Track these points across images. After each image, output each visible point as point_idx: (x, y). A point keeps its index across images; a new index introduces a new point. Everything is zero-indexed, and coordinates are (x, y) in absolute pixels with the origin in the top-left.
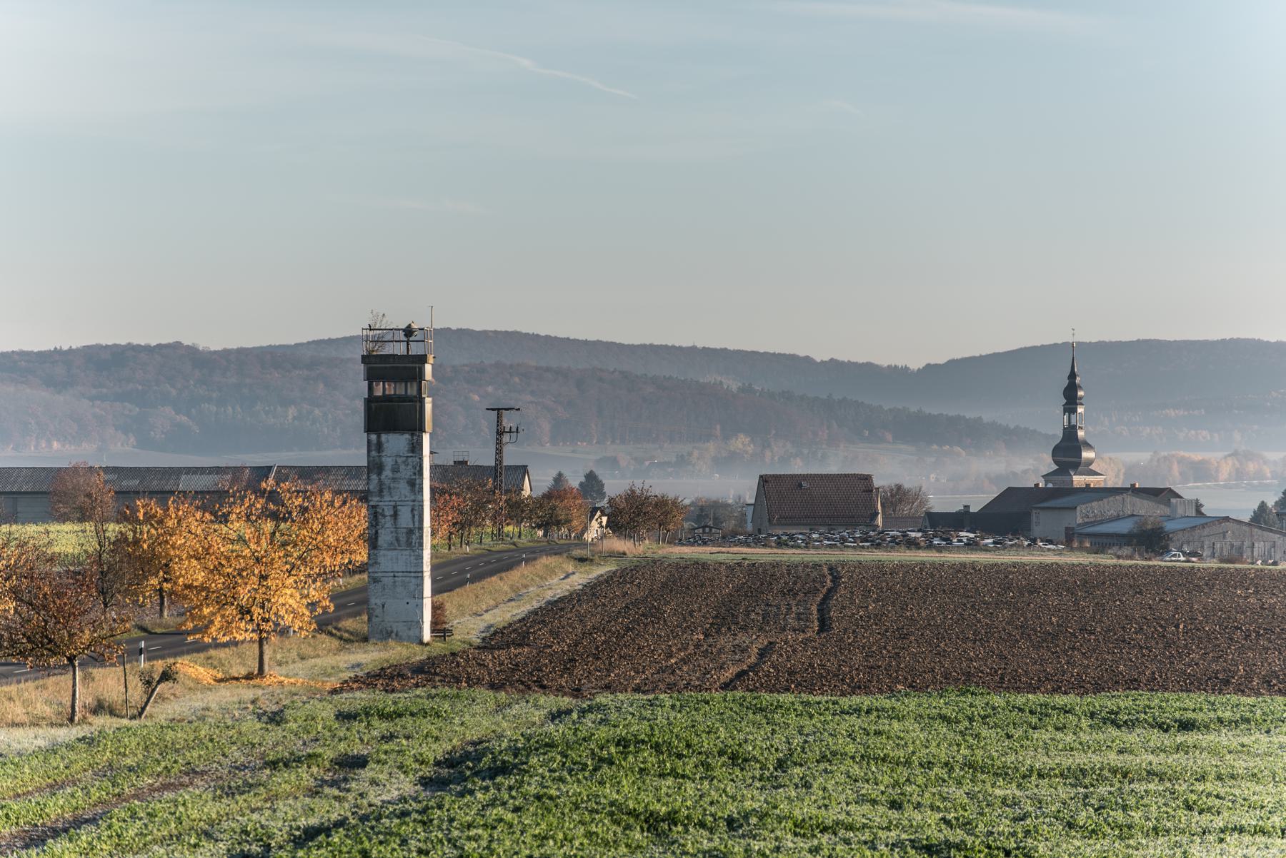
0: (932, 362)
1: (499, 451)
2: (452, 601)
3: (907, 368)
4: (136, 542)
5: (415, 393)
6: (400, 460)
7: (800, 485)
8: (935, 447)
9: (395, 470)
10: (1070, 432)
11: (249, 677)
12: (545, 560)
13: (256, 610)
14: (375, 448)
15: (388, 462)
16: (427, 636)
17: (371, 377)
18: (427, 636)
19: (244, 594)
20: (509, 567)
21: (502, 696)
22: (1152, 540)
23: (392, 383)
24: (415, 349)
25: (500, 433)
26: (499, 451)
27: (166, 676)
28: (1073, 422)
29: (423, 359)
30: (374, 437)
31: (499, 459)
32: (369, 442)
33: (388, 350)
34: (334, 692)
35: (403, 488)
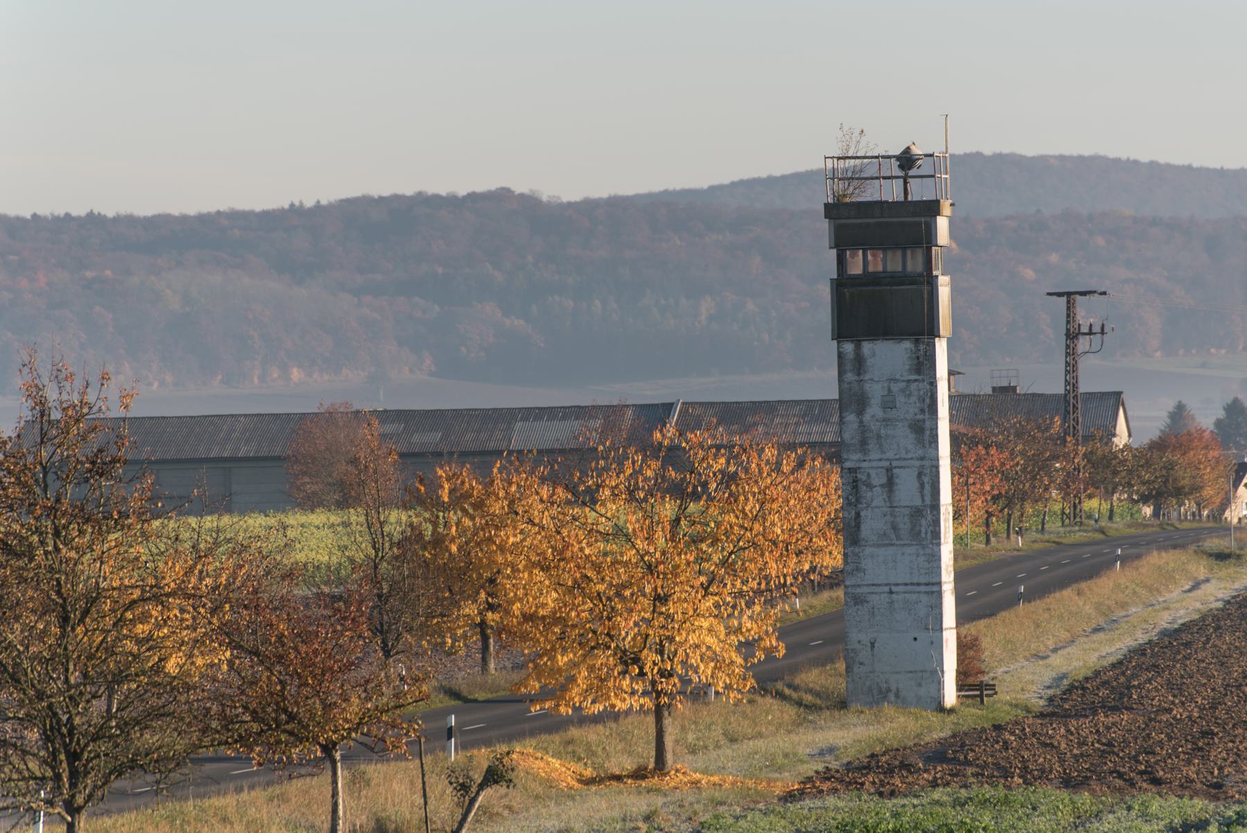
1: (1071, 368)
2: (992, 634)
4: (438, 542)
6: (895, 388)
11: (639, 774)
12: (1156, 559)
13: (649, 657)
15: (875, 392)
16: (950, 696)
17: (843, 241)
18: (950, 696)
19: (627, 630)
20: (1093, 571)
21: (1085, 799)
22: (843, 725)
23: (876, 249)
24: (920, 191)
25: (1072, 336)
26: (1071, 368)
27: (494, 776)
29: (933, 208)
30: (849, 347)
31: (1072, 384)
33: (871, 193)
34: (789, 797)
35: (904, 438)
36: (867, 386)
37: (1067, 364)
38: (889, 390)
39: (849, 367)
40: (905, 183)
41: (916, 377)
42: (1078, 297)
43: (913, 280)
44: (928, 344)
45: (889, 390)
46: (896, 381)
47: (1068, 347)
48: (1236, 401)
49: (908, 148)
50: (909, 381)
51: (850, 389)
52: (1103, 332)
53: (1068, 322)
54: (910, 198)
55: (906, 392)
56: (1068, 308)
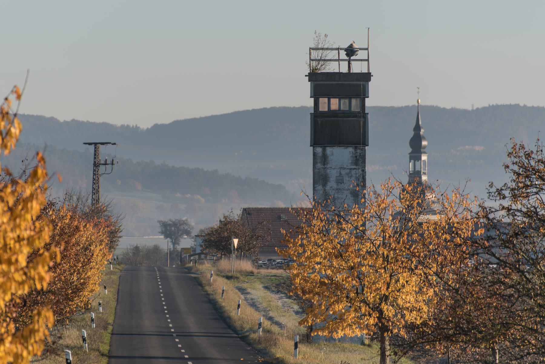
0: (160, 122)
3: (137, 128)
5: (358, 110)
6: (344, 172)
7: (280, 218)
8: (178, 195)
9: (340, 181)
10: (415, 175)
14: (320, 162)
15: (333, 174)
24: (358, 68)
28: (417, 168)
30: (319, 150)
32: (315, 154)
33: (332, 68)
36: (328, 171)
37: (94, 179)
38: (340, 173)
39: (319, 160)
40: (349, 64)
41: (355, 167)
42: (100, 146)
43: (355, 115)
44: (362, 150)
45: (340, 173)
46: (344, 168)
47: (94, 170)
48: (245, 210)
49: (352, 45)
50: (351, 169)
51: (319, 172)
52: (112, 164)
53: (95, 158)
54: (351, 72)
55: (349, 175)
56: (95, 151)
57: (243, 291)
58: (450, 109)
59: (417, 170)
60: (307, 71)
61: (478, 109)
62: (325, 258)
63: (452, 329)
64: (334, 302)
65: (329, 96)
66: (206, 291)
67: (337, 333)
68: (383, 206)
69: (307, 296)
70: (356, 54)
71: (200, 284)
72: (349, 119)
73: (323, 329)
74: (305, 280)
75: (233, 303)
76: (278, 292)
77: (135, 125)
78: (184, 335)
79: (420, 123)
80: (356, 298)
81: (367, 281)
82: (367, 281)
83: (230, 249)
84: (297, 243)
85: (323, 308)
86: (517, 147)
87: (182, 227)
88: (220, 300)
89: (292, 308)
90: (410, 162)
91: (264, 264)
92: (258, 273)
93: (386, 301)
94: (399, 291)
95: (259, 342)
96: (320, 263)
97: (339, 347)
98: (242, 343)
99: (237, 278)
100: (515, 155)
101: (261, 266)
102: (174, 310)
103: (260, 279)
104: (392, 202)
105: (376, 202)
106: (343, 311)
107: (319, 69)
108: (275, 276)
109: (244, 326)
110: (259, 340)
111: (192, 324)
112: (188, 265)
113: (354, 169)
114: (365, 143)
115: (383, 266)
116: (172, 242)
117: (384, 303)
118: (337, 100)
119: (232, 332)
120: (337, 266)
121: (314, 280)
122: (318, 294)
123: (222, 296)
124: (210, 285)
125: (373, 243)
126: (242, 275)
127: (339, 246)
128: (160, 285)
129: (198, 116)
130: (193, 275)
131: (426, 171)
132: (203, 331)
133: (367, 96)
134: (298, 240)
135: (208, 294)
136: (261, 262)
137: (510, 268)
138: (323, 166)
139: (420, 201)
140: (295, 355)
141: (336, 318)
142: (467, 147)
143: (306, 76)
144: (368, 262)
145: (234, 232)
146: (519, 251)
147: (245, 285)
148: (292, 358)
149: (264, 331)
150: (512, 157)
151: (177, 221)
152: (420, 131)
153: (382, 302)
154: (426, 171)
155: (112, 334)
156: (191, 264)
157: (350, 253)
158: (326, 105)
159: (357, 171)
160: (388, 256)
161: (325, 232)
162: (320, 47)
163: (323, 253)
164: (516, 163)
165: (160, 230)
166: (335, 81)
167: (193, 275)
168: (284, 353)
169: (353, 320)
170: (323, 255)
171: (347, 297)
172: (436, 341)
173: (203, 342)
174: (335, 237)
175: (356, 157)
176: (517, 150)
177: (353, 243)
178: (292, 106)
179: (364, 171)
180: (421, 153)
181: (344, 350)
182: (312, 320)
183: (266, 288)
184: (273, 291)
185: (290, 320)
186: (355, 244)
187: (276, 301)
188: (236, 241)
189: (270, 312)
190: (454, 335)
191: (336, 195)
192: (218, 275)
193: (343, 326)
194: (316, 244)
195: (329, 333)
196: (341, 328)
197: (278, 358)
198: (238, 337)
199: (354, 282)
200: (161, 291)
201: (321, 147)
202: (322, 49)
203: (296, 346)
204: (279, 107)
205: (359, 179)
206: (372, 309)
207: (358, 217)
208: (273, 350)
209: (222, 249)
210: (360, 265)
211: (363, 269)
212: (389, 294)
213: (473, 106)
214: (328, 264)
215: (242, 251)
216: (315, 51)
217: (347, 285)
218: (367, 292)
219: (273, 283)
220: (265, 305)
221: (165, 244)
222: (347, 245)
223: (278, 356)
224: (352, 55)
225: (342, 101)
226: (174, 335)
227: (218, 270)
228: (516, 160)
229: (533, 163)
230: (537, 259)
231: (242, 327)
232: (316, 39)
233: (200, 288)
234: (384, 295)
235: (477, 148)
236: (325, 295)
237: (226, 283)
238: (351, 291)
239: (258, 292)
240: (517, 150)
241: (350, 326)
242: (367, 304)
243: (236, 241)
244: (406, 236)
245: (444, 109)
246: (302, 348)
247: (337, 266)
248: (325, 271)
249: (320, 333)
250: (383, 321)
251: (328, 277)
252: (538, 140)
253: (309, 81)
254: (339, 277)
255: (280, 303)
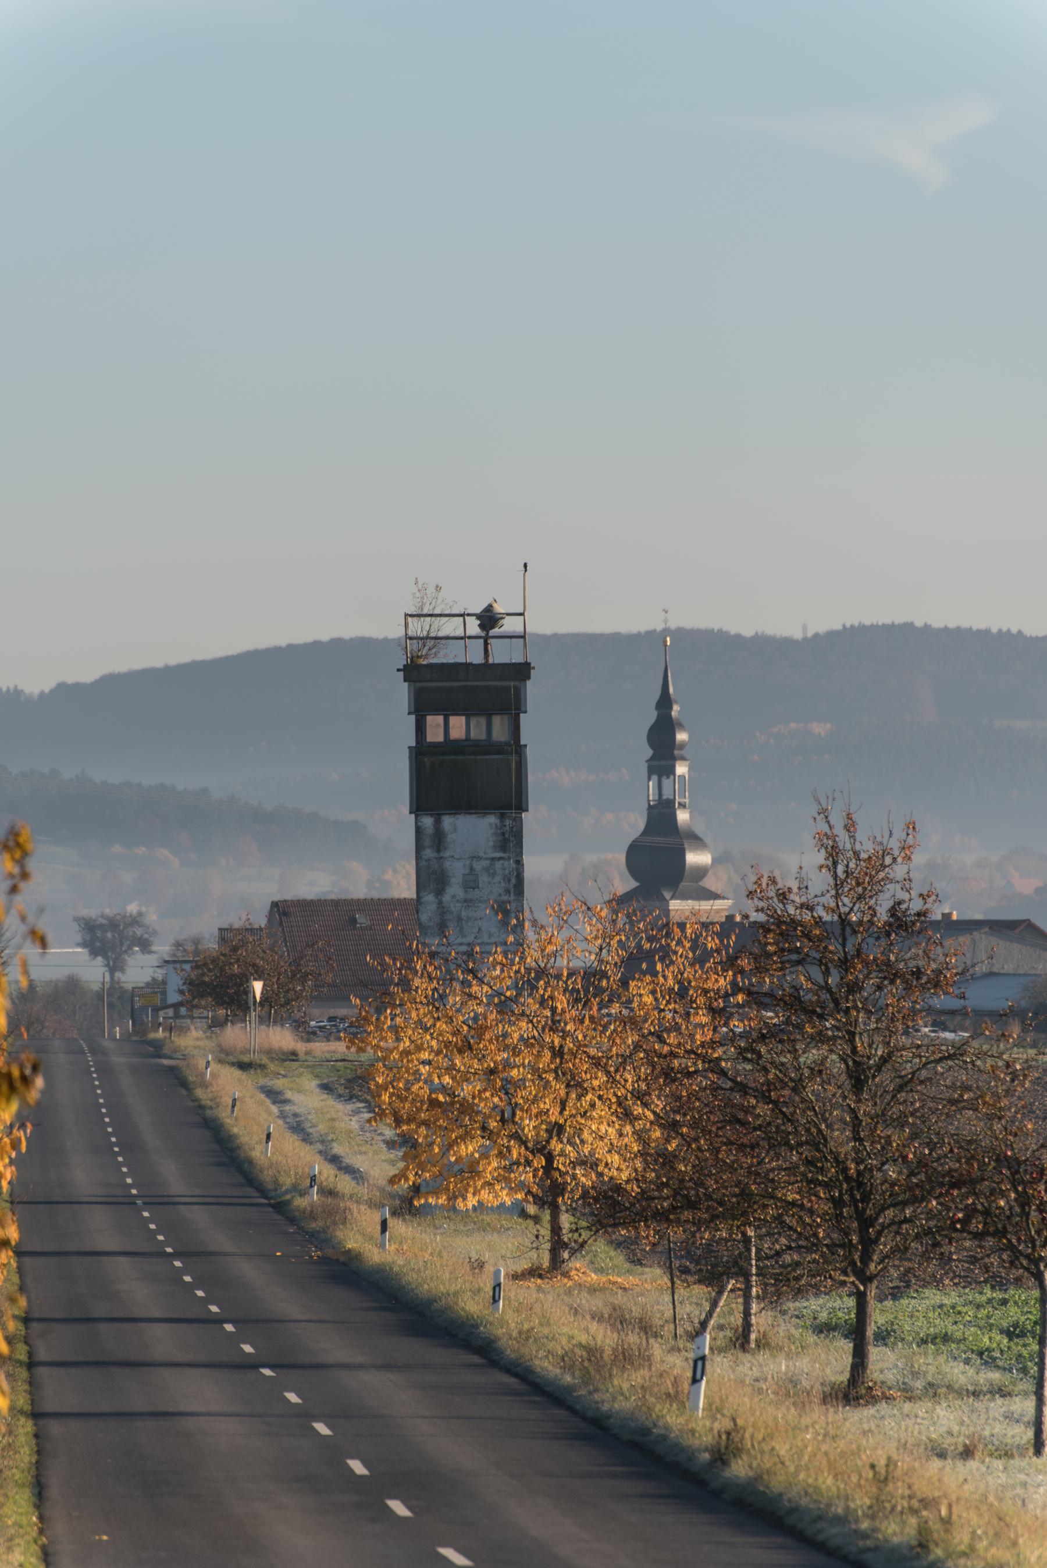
0: (70, 679)
3: (17, 693)
6: (478, 866)
7: (353, 921)
9: (470, 883)
10: (661, 815)
14: (430, 846)
15: (456, 869)
23: (467, 721)
24: (502, 654)
28: (667, 794)
30: (428, 821)
32: (418, 830)
36: (447, 864)
39: (427, 842)
40: (486, 644)
43: (498, 749)
44: (515, 820)
46: (479, 858)
48: (275, 905)
49: (490, 606)
50: (493, 859)
54: (491, 661)
57: (274, 1096)
58: (752, 638)
59: (665, 797)
60: (401, 663)
61: (816, 636)
62: (438, 1053)
63: (668, 1198)
64: (456, 1138)
65: (447, 710)
66: (197, 1100)
67: (465, 1199)
68: (550, 949)
69: (405, 1128)
70: (500, 623)
71: (184, 1084)
72: (488, 757)
73: (436, 1193)
74: (399, 1097)
75: (255, 1128)
76: (351, 1098)
77: (12, 687)
78: (160, 1202)
79: (671, 691)
80: (500, 1131)
81: (522, 1097)
82: (522, 1097)
83: (247, 1003)
84: (384, 1023)
85: (437, 1150)
86: (764, 881)
87: (130, 931)
88: (228, 1121)
89: (381, 1134)
90: (649, 779)
91: (320, 1027)
92: (307, 1053)
93: (559, 1135)
94: (584, 1115)
95: (313, 1216)
96: (429, 1063)
97: (475, 1223)
98: (277, 1217)
99: (262, 1067)
100: (759, 896)
101: (314, 1033)
102: (132, 1146)
103: (315, 1067)
104: (568, 942)
105: (537, 941)
106: (477, 1155)
107: (426, 656)
108: (344, 1060)
109: (281, 1179)
110: (312, 1212)
111: (173, 1178)
112: (152, 1036)
113: (501, 858)
114: (521, 806)
115: (553, 1066)
116: (107, 965)
117: (555, 1139)
118: (463, 718)
119: (256, 1194)
120: (462, 1068)
121: (417, 1095)
122: (425, 1123)
123: (233, 1111)
124: (205, 1085)
125: (531, 1021)
126: (272, 1059)
127: (465, 1028)
128: (98, 1087)
129: (159, 664)
130: (166, 1062)
131: (687, 801)
132: (198, 1192)
133: (523, 709)
134: (386, 1018)
135: (201, 1107)
136: (313, 1023)
137: (755, 1097)
138: (436, 855)
139: (623, 938)
140: (382, 1246)
141: (462, 1171)
142: (793, 725)
143: (398, 670)
144: (524, 1059)
145: (254, 965)
146: (769, 1066)
147: (279, 1083)
148: (376, 1250)
149: (322, 1191)
150: (756, 900)
151: (118, 917)
152: (671, 708)
153: (551, 1137)
154: (687, 801)
155: (12, 1203)
156: (161, 1034)
157: (487, 1044)
158: (441, 731)
159: (506, 863)
160: (561, 1046)
161: (437, 1001)
162: (425, 611)
163: (434, 1043)
164: (762, 910)
165: (79, 938)
166: (458, 681)
167: (166, 1062)
168: (360, 1238)
169: (496, 1174)
170: (435, 1047)
171: (484, 1128)
172: (639, 1221)
173: (199, 1217)
174: (458, 1011)
175: (503, 834)
176: (764, 886)
177: (494, 1023)
178: (381, 636)
179: (519, 863)
180: (674, 759)
181: (484, 1228)
182: (416, 1174)
183: (326, 1088)
184: (340, 1096)
185: (379, 1164)
186: (497, 1025)
187: (344, 1118)
188: (258, 986)
189: (335, 1145)
190: (673, 1209)
191: (464, 913)
192: (220, 1061)
193: (475, 1187)
194: (419, 1023)
195: (449, 1199)
196: (471, 1190)
197: (349, 1251)
198: (270, 1205)
199: (496, 1100)
200: (101, 1101)
201: (431, 815)
202: (431, 615)
203: (384, 1225)
204: (351, 639)
205: (509, 880)
206: (532, 1152)
207: (502, 971)
208: (340, 1234)
209: (227, 1003)
210: (507, 1065)
211: (514, 1073)
212: (565, 1121)
213: (805, 628)
214: (446, 1063)
215: (271, 1007)
216: (415, 619)
217: (482, 1105)
218: (522, 1119)
219: (340, 1077)
220: (322, 1128)
221: (93, 973)
222: (481, 1028)
223: (350, 1245)
224: (493, 627)
225: (474, 721)
226: (139, 1202)
227: (219, 1046)
228: (761, 904)
229: (791, 910)
230: (801, 1079)
231: (276, 1182)
232: (418, 595)
233: (184, 1092)
234: (556, 1123)
235: (818, 728)
236: (440, 1127)
237: (239, 1080)
238: (490, 1116)
239: (308, 1098)
240: (764, 886)
241: (490, 1184)
242: (523, 1142)
243: (258, 986)
244: (595, 1008)
245: (738, 636)
246: (397, 1226)
247: (462, 1068)
248: (439, 1077)
249: (430, 1200)
250: (556, 1174)
251: (444, 1089)
252: (801, 868)
253: (405, 681)
254: (466, 1091)
255: (354, 1124)
